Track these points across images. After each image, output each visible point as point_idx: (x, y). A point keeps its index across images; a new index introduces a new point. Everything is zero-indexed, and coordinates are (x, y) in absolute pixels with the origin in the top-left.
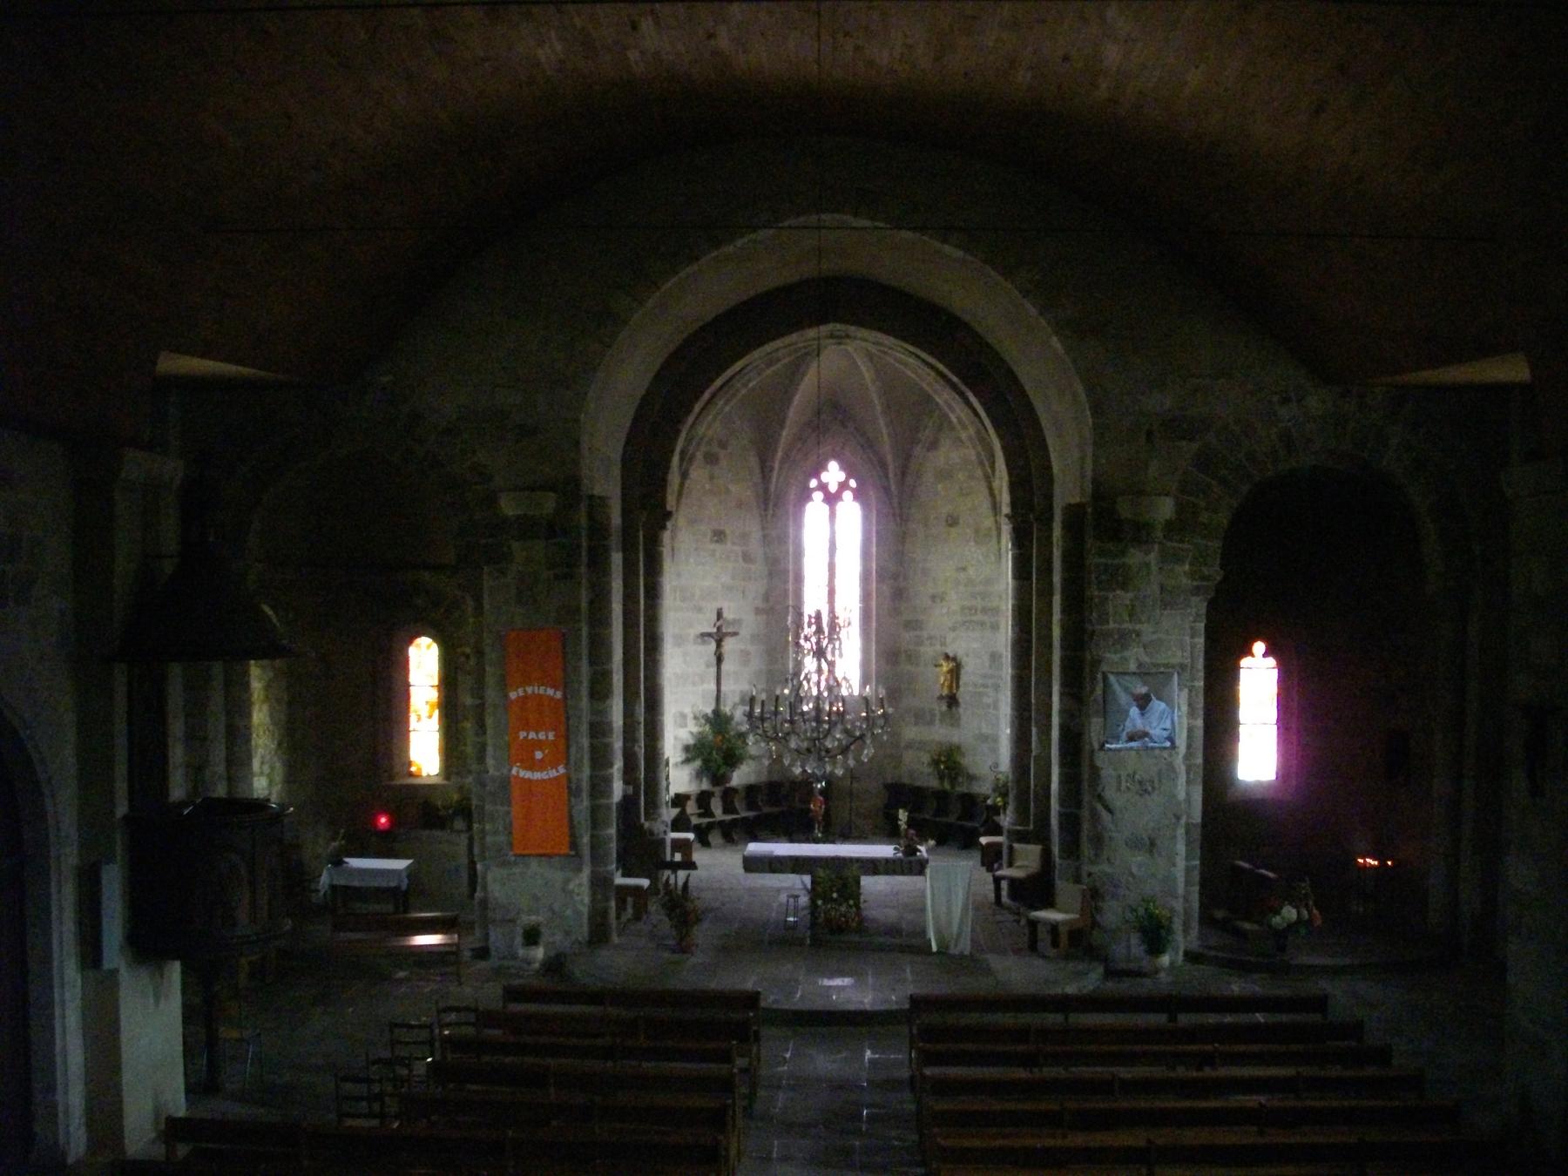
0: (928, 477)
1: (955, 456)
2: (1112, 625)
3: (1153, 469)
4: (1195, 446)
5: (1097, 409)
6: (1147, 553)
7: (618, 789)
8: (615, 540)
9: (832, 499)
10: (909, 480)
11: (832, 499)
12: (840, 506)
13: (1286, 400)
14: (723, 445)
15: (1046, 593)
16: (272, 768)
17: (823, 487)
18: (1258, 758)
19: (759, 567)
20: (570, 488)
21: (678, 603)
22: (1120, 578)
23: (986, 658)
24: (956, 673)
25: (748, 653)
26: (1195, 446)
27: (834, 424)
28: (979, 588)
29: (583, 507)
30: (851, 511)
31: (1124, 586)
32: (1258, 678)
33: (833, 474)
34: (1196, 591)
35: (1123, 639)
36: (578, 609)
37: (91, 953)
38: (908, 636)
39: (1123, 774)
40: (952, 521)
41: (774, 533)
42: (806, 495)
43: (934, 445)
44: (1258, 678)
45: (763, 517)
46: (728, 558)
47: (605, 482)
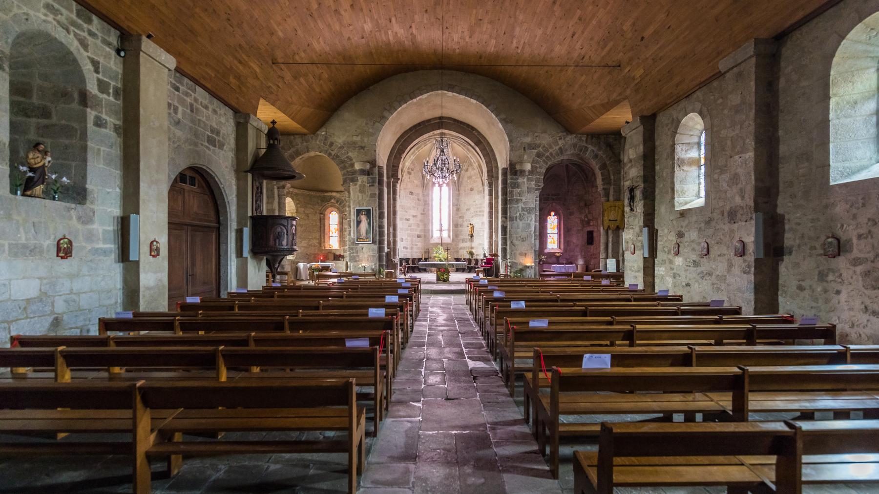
1: (472, 173)
3: (525, 157)
5: (511, 141)
7: (386, 250)
8: (385, 184)
9: (440, 186)
13: (560, 139)
15: (497, 198)
18: (553, 244)
19: (422, 202)
20: (373, 163)
22: (516, 185)
24: (473, 228)
27: (441, 167)
30: (445, 188)
32: (552, 222)
34: (537, 190)
35: (518, 201)
37: (239, 253)
40: (472, 190)
43: (467, 170)
44: (552, 222)
47: (382, 159)
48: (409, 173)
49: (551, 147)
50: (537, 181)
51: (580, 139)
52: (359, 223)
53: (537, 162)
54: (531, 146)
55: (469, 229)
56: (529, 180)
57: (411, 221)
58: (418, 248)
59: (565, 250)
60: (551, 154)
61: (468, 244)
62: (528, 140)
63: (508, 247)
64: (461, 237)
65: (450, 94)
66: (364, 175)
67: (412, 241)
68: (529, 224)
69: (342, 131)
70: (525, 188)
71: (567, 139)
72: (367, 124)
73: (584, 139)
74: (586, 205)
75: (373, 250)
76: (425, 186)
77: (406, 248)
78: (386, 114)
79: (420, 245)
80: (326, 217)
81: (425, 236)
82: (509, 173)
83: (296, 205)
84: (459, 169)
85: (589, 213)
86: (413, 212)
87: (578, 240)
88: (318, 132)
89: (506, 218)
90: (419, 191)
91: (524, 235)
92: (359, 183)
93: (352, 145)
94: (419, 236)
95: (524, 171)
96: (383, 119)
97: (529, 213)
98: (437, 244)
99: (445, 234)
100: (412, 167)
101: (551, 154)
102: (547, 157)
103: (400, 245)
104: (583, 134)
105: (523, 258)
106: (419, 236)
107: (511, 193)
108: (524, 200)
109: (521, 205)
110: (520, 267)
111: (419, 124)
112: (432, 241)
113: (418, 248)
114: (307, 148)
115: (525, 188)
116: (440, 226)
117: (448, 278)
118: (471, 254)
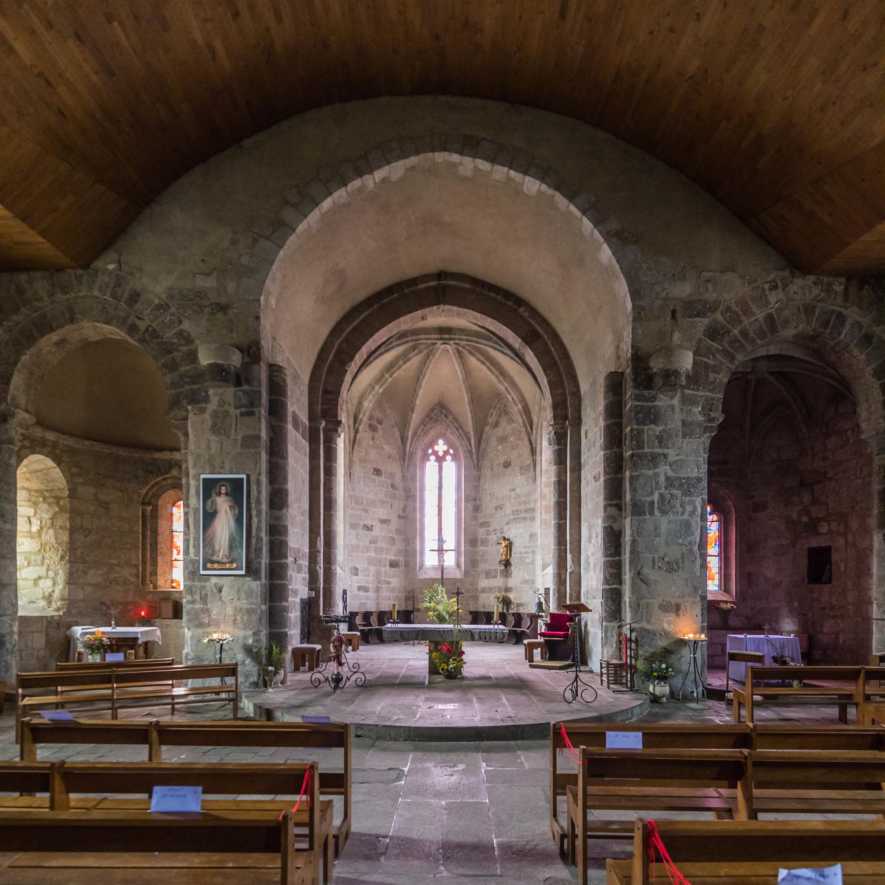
0: (493, 442)
1: (508, 429)
2: (646, 450)
3: (676, 337)
4: (706, 321)
6: (672, 398)
9: (440, 460)
10: (483, 446)
11: (440, 460)
12: (444, 464)
13: (774, 288)
14: (380, 422)
16: (56, 574)
17: (435, 453)
19: (400, 493)
20: (252, 351)
21: (353, 505)
22: (650, 416)
23: (527, 537)
24: (510, 546)
25: (393, 539)
26: (706, 321)
28: (523, 499)
29: (263, 367)
30: (449, 466)
31: (654, 422)
33: (441, 447)
34: (706, 429)
35: (655, 460)
36: (258, 437)
38: (482, 531)
39: (656, 557)
40: (507, 465)
41: (409, 475)
42: (426, 457)
43: (497, 425)
45: (402, 466)
46: (382, 486)
48: (373, 428)
49: (747, 311)
50: (708, 408)
51: (829, 289)
52: (210, 517)
53: (710, 352)
54: (693, 308)
55: (502, 549)
56: (685, 400)
57: (377, 532)
58: (392, 590)
59: (742, 596)
60: (744, 333)
61: (498, 582)
62: (684, 290)
63: (627, 589)
64: (483, 567)
65: (467, 164)
66: (225, 380)
67: (378, 574)
68: (688, 524)
69: (163, 261)
70: (675, 422)
71: (792, 288)
72: (234, 242)
73: (839, 288)
74: (802, 484)
75: (249, 594)
76: (408, 459)
77: (365, 589)
78: (288, 214)
79: (395, 582)
80: (162, 512)
81: (407, 564)
82: (629, 384)
83: (70, 478)
84: (487, 408)
85: (815, 501)
86: (381, 512)
87: (779, 570)
88: (98, 264)
89: (619, 508)
90: (394, 467)
91: (674, 553)
92: (213, 405)
93: (193, 301)
94: (393, 564)
95: (676, 373)
96: (280, 229)
97: (687, 493)
98: (434, 580)
99: (450, 560)
100: (378, 414)
101: (744, 333)
102: (734, 341)
103: (343, 580)
104: (836, 273)
105: (671, 617)
106: (393, 564)
107: (637, 437)
108: (672, 457)
109: (664, 470)
110: (662, 643)
111: (389, 290)
112: (422, 576)
113: (392, 590)
114: (71, 310)
115: (675, 422)
116: (440, 542)
117: (458, 670)
118: (507, 602)
